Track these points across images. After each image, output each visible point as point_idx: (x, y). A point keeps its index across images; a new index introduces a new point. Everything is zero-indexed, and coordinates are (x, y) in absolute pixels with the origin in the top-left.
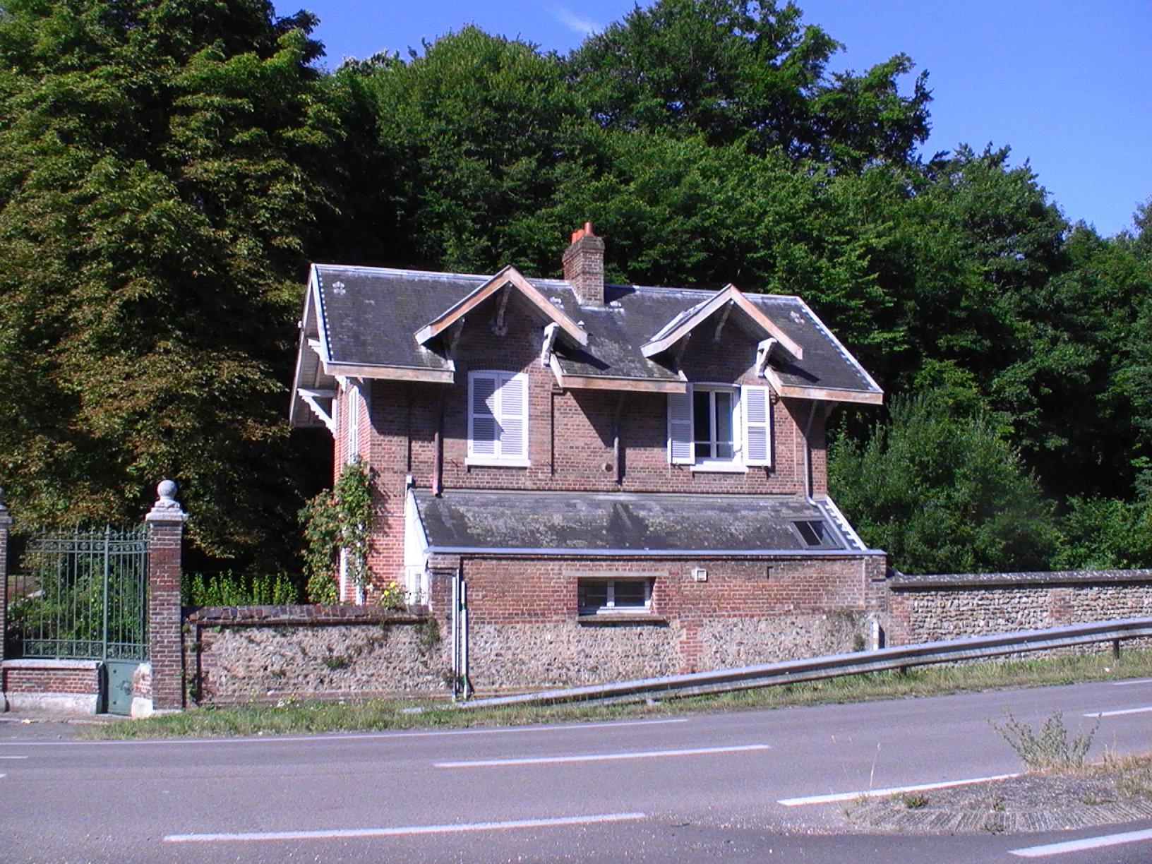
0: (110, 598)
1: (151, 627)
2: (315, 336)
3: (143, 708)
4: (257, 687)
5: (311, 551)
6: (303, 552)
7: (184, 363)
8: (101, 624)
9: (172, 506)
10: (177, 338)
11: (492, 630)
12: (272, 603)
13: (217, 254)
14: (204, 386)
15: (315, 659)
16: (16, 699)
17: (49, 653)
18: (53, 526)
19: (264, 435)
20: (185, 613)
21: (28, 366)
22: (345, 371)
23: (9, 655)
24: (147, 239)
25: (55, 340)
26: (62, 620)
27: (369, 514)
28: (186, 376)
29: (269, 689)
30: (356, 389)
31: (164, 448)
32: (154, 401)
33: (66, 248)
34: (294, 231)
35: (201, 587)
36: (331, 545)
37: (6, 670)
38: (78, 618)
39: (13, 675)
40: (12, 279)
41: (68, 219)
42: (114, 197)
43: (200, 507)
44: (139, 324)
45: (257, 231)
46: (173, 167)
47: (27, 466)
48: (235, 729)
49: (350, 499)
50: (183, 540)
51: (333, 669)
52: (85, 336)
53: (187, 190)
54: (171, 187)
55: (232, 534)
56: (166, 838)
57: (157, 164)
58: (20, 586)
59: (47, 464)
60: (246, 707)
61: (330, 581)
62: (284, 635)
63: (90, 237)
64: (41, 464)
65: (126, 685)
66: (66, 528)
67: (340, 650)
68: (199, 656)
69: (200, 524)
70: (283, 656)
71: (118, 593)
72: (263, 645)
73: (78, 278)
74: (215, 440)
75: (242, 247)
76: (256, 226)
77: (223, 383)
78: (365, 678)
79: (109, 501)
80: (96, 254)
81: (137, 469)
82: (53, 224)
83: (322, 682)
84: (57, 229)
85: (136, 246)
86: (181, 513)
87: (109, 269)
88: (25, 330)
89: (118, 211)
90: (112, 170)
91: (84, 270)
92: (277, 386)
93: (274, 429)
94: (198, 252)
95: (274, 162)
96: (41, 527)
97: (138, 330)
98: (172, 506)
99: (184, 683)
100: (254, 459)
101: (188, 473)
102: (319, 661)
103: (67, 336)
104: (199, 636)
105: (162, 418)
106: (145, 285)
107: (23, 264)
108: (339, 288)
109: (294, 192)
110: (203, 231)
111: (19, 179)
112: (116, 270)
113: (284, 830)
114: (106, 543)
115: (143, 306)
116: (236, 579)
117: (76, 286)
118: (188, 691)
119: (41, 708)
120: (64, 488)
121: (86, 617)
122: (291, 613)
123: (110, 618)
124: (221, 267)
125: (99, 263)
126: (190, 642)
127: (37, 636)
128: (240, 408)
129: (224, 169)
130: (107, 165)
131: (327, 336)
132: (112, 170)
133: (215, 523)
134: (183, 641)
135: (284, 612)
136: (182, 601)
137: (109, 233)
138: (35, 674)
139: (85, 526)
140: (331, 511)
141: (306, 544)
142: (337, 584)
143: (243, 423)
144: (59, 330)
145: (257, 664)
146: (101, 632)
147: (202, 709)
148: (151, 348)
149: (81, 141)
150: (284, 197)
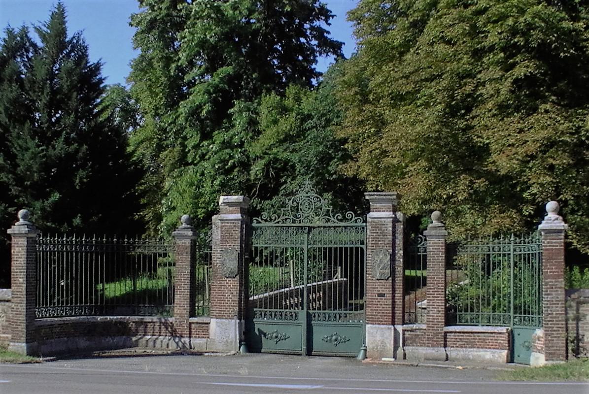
1: (544, 304)
3: (538, 360)
7: (559, 118)
8: (509, 302)
9: (557, 219)
10: (553, 102)
16: (453, 353)
17: (474, 322)
18: (475, 236)
20: (568, 293)
23: (448, 323)
24: (525, 34)
25: (469, 110)
26: (483, 300)
28: (561, 128)
31: (549, 179)
32: (540, 147)
33: (470, 47)
35: (578, 275)
37: (446, 333)
38: (494, 298)
39: (449, 336)
40: (437, 71)
43: (575, 219)
44: (525, 94)
52: (489, 105)
58: (455, 277)
59: (470, 194)
63: (486, 37)
64: (465, 194)
65: (526, 344)
66: (484, 237)
68: (577, 324)
69: (576, 231)
71: (520, 280)
79: (512, 218)
80: (492, 49)
81: (531, 195)
84: (464, 34)
85: (519, 40)
86: (563, 224)
87: (501, 58)
88: (448, 105)
89: (503, 17)
91: (485, 60)
96: (467, 237)
97: (527, 96)
98: (557, 219)
99: (567, 343)
101: (567, 196)
103: (477, 106)
104: (578, 310)
106: (527, 67)
110: (565, 24)
114: (511, 246)
115: (528, 81)
117: (480, 72)
118: (570, 348)
119: (469, 359)
120: (481, 210)
123: (515, 298)
125: (494, 54)
126: (571, 314)
127: (466, 311)
136: (565, 285)
137: (499, 33)
138: (461, 336)
144: (470, 103)
146: (509, 307)
147: (580, 361)
148: (535, 110)
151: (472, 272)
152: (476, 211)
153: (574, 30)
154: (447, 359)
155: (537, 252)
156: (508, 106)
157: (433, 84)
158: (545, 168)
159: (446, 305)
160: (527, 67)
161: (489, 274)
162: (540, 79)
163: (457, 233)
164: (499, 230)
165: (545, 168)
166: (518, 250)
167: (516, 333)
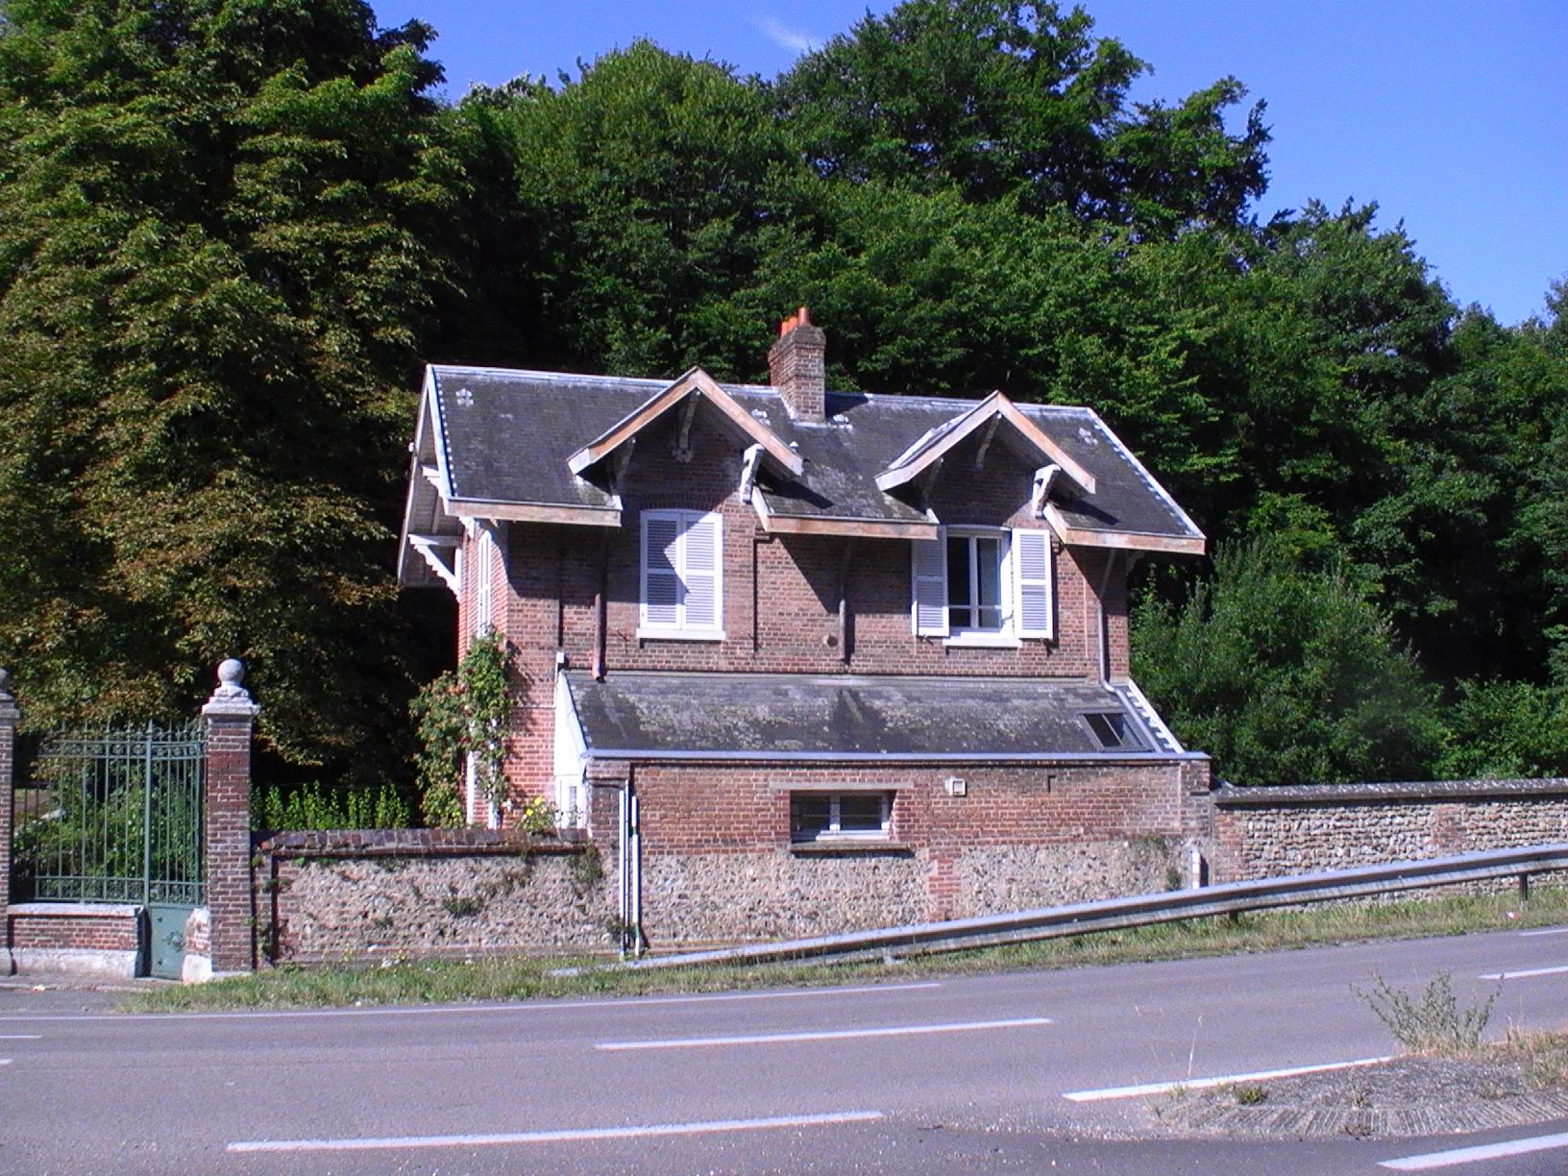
1: (209, 860)
2: (432, 463)
3: (198, 969)
4: (354, 941)
5: (427, 756)
6: (417, 756)
7: (253, 499)
8: (142, 855)
9: (238, 695)
10: (245, 467)
11: (673, 863)
12: (373, 827)
13: (297, 350)
15: (433, 902)
16: (26, 958)
17: (70, 895)
18: (75, 722)
19: (363, 598)
20: (256, 840)
21: (41, 504)
22: (473, 511)
24: (202, 331)
25: (78, 470)
27: (506, 705)
28: (256, 517)
29: (370, 944)
30: (488, 535)
32: (213, 552)
33: (92, 344)
34: (404, 320)
35: (278, 805)
37: (12, 917)
38: (110, 846)
39: (21, 925)
40: (20, 386)
42: (158, 274)
43: (275, 696)
45: (353, 321)
46: (237, 233)
47: (40, 641)
48: (323, 997)
49: (479, 684)
50: (252, 741)
51: (457, 916)
52: (120, 464)
53: (258, 264)
54: (236, 261)
55: (319, 733)
56: (230, 1147)
57: (217, 229)
58: (32, 803)
60: (338, 968)
61: (453, 796)
62: (391, 870)
63: (126, 328)
65: (175, 939)
66: (94, 725)
67: (466, 890)
68: (274, 899)
69: (276, 719)
70: (389, 898)
71: (164, 812)
72: (361, 884)
73: (110, 384)
75: (332, 342)
76: (351, 313)
77: (306, 527)
78: (500, 928)
80: (134, 352)
81: (190, 644)
83: (442, 933)
84: (81, 318)
85: (188, 341)
86: (250, 704)
88: (37, 456)
89: (162, 293)
91: (118, 373)
92: (380, 531)
93: (376, 589)
95: (376, 227)
97: (191, 455)
98: (238, 695)
99: (254, 936)
100: (347, 629)
101: (261, 650)
103: (94, 464)
104: (275, 871)
106: (201, 394)
107: (35, 366)
108: (464, 398)
110: (280, 320)
111: (29, 250)
112: (162, 373)
113: (390, 1136)
114: (148, 746)
115: (198, 423)
116: (325, 793)
117: (106, 396)
119: (59, 971)
121: (121, 846)
122: (400, 840)
123: (153, 848)
124: (305, 370)
125: (138, 365)
126: (262, 880)
127: (54, 872)
128: (330, 561)
129: (308, 236)
130: (149, 231)
131: (448, 463)
133: (297, 718)
135: (390, 838)
138: (51, 924)
139: (119, 723)
140: (454, 701)
141: (420, 746)
142: (462, 800)
143: (334, 581)
144: (84, 455)
146: (141, 866)
147: (280, 972)
148: (207, 479)
149: (113, 198)
150: (390, 273)
151: (67, 793)
152: (79, 671)
153: (298, 333)
154: (14, 970)
155: (198, 757)
156: (157, 468)
157: (10, 410)
158: (220, 594)
159: (11, 861)
160: (201, 394)
161: (101, 799)
162: (221, 420)
163: (39, 714)
164: (125, 711)
165: (220, 594)
166: (160, 752)
167: (154, 916)
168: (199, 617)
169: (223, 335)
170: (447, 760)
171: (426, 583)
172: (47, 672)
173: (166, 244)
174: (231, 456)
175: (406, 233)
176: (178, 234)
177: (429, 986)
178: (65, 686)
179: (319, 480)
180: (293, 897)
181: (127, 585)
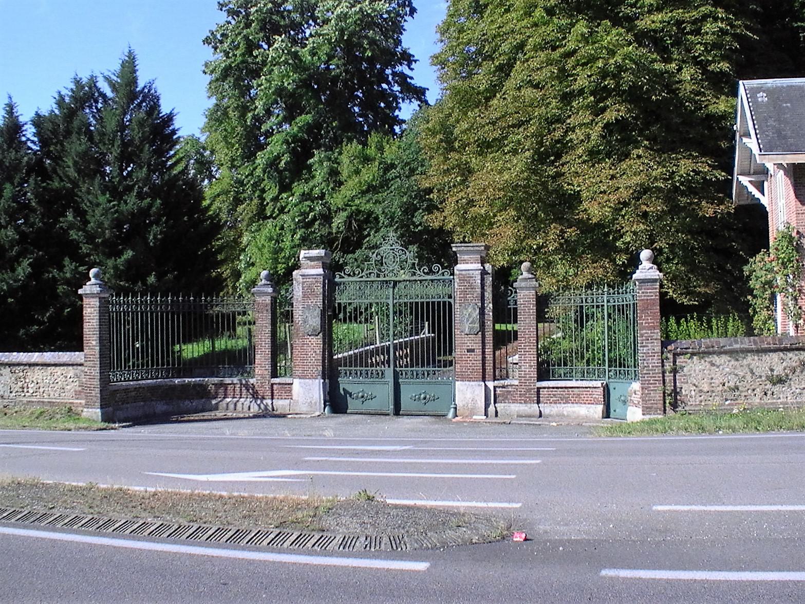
0: (610, 337)
1: (640, 356)
2: (748, 135)
3: (635, 414)
4: (717, 398)
5: (755, 297)
6: (749, 297)
8: (604, 355)
9: (651, 268)
12: (726, 336)
13: (668, 83)
14: (668, 180)
15: (761, 377)
16: (546, 409)
17: (568, 376)
18: (567, 288)
19: (715, 212)
20: (664, 345)
21: (541, 176)
22: (772, 160)
25: (558, 156)
27: (797, 266)
28: (654, 173)
29: (726, 400)
30: (782, 172)
31: (642, 227)
33: (559, 90)
34: (724, 58)
35: (675, 326)
36: (769, 292)
37: (539, 389)
38: (588, 351)
40: (525, 117)
41: (559, 69)
42: (589, 49)
43: (670, 268)
45: (696, 62)
46: (629, 22)
47: (546, 246)
48: (702, 429)
49: (782, 256)
50: (660, 293)
51: (774, 384)
52: (580, 151)
53: (641, 38)
54: (630, 37)
55: (695, 287)
56: (654, 508)
57: (617, 22)
58: (547, 330)
60: (709, 413)
61: (769, 318)
62: (737, 360)
63: (576, 80)
64: (556, 244)
65: (622, 398)
66: (576, 288)
67: (779, 370)
68: (675, 376)
69: (671, 280)
70: (737, 375)
71: (615, 333)
72: (721, 367)
73: (570, 110)
74: (678, 218)
75: (687, 74)
76: (695, 58)
77: (682, 176)
78: (798, 391)
79: (606, 268)
80: (581, 92)
81: (624, 243)
82: (549, 74)
83: (766, 394)
84: (552, 78)
85: (609, 83)
86: (658, 273)
88: (537, 152)
89: (592, 59)
90: (585, 30)
91: (574, 104)
92: (721, 175)
93: (722, 207)
94: (654, 82)
95: (703, 9)
96: (559, 289)
97: (618, 142)
98: (651, 268)
100: (706, 229)
101: (661, 244)
102: (763, 379)
103: (567, 152)
104: (674, 362)
105: (640, 205)
107: (531, 105)
108: (762, 97)
109: (721, 30)
110: (656, 66)
111: (521, 46)
112: (598, 102)
113: (740, 504)
114: (605, 298)
115: (620, 125)
116: (700, 319)
117: (569, 117)
118: (667, 401)
119: (563, 415)
121: (593, 351)
122: (742, 343)
123: (610, 351)
124: (673, 92)
125: (584, 99)
126: (668, 366)
127: (559, 365)
128: (696, 194)
129: (666, 19)
130: (582, 27)
131: (756, 134)
132: (585, 30)
133: (682, 279)
134: (663, 366)
135: (736, 342)
136: (661, 337)
137: (588, 76)
138: (555, 392)
139: (589, 286)
140: (768, 266)
141: (751, 291)
142: (775, 320)
143: (698, 204)
144: (560, 149)
145: (717, 381)
146: (604, 361)
147: (678, 415)
148: (627, 155)
149: (560, 13)
150: (713, 33)
153: (667, 72)
155: (632, 303)
156: (599, 152)
157: (521, 129)
159: (538, 360)
160: (618, 111)
161: (582, 326)
163: (548, 284)
168: (628, 229)
169: (627, 77)
170: (765, 299)
171: (749, 202)
172: (551, 263)
173: (591, 33)
174: (637, 142)
175: (719, 9)
176: (597, 27)
177: (759, 423)
178: (560, 269)
179: (686, 150)
180: (685, 375)
181: (589, 215)
